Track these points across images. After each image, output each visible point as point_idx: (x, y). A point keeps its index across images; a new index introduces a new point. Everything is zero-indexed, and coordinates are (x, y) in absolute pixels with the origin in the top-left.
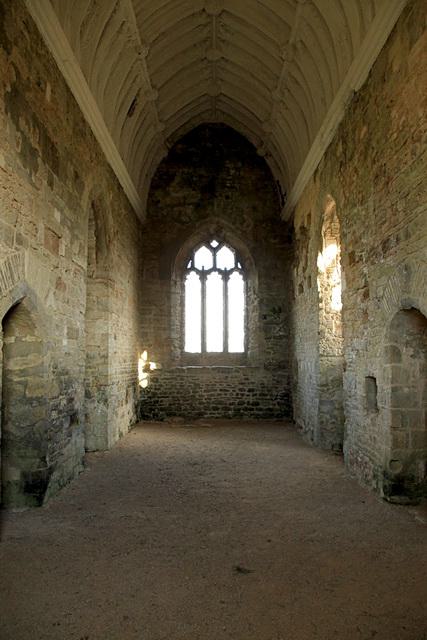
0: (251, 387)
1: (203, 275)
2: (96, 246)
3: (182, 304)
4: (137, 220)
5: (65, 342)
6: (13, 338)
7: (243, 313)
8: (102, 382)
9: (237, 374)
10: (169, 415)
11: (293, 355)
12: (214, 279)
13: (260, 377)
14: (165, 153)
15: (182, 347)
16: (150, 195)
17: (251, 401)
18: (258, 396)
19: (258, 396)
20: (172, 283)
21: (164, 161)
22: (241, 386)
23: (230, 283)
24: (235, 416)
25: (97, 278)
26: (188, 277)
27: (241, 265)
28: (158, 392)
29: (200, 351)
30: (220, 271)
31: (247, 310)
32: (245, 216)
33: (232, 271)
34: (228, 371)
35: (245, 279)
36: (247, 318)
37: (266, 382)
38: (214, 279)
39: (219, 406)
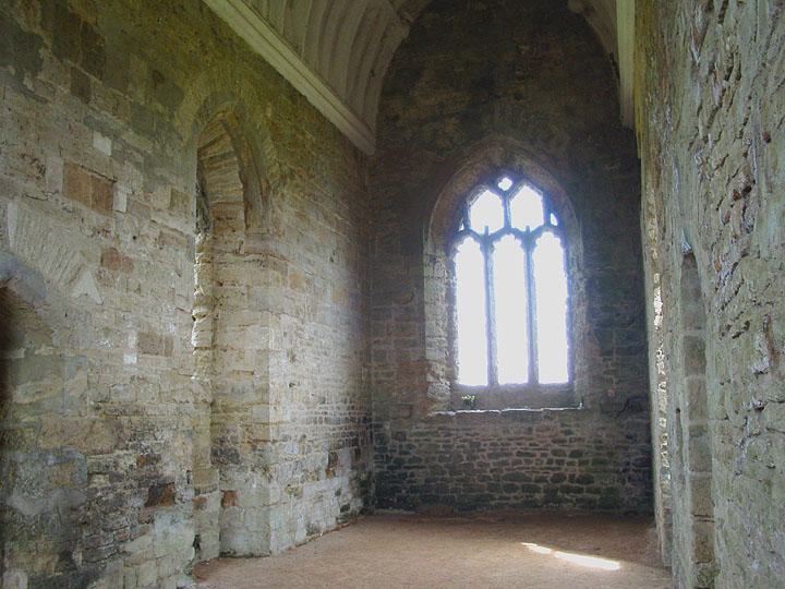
0: (576, 446)
1: (487, 241)
2: (246, 200)
3: (450, 297)
4: (356, 153)
5: (131, 359)
6: (23, 350)
8: (259, 434)
9: (547, 423)
11: (424, 365)
12: (508, 247)
13: (589, 430)
14: (402, 33)
15: (451, 377)
16: (382, 108)
17: (578, 474)
20: (426, 260)
21: (404, 46)
24: (546, 502)
25: (248, 253)
26: (460, 247)
28: (406, 458)
29: (485, 383)
30: (517, 233)
33: (539, 231)
34: (534, 416)
35: (565, 244)
38: (508, 247)
39: (518, 484)
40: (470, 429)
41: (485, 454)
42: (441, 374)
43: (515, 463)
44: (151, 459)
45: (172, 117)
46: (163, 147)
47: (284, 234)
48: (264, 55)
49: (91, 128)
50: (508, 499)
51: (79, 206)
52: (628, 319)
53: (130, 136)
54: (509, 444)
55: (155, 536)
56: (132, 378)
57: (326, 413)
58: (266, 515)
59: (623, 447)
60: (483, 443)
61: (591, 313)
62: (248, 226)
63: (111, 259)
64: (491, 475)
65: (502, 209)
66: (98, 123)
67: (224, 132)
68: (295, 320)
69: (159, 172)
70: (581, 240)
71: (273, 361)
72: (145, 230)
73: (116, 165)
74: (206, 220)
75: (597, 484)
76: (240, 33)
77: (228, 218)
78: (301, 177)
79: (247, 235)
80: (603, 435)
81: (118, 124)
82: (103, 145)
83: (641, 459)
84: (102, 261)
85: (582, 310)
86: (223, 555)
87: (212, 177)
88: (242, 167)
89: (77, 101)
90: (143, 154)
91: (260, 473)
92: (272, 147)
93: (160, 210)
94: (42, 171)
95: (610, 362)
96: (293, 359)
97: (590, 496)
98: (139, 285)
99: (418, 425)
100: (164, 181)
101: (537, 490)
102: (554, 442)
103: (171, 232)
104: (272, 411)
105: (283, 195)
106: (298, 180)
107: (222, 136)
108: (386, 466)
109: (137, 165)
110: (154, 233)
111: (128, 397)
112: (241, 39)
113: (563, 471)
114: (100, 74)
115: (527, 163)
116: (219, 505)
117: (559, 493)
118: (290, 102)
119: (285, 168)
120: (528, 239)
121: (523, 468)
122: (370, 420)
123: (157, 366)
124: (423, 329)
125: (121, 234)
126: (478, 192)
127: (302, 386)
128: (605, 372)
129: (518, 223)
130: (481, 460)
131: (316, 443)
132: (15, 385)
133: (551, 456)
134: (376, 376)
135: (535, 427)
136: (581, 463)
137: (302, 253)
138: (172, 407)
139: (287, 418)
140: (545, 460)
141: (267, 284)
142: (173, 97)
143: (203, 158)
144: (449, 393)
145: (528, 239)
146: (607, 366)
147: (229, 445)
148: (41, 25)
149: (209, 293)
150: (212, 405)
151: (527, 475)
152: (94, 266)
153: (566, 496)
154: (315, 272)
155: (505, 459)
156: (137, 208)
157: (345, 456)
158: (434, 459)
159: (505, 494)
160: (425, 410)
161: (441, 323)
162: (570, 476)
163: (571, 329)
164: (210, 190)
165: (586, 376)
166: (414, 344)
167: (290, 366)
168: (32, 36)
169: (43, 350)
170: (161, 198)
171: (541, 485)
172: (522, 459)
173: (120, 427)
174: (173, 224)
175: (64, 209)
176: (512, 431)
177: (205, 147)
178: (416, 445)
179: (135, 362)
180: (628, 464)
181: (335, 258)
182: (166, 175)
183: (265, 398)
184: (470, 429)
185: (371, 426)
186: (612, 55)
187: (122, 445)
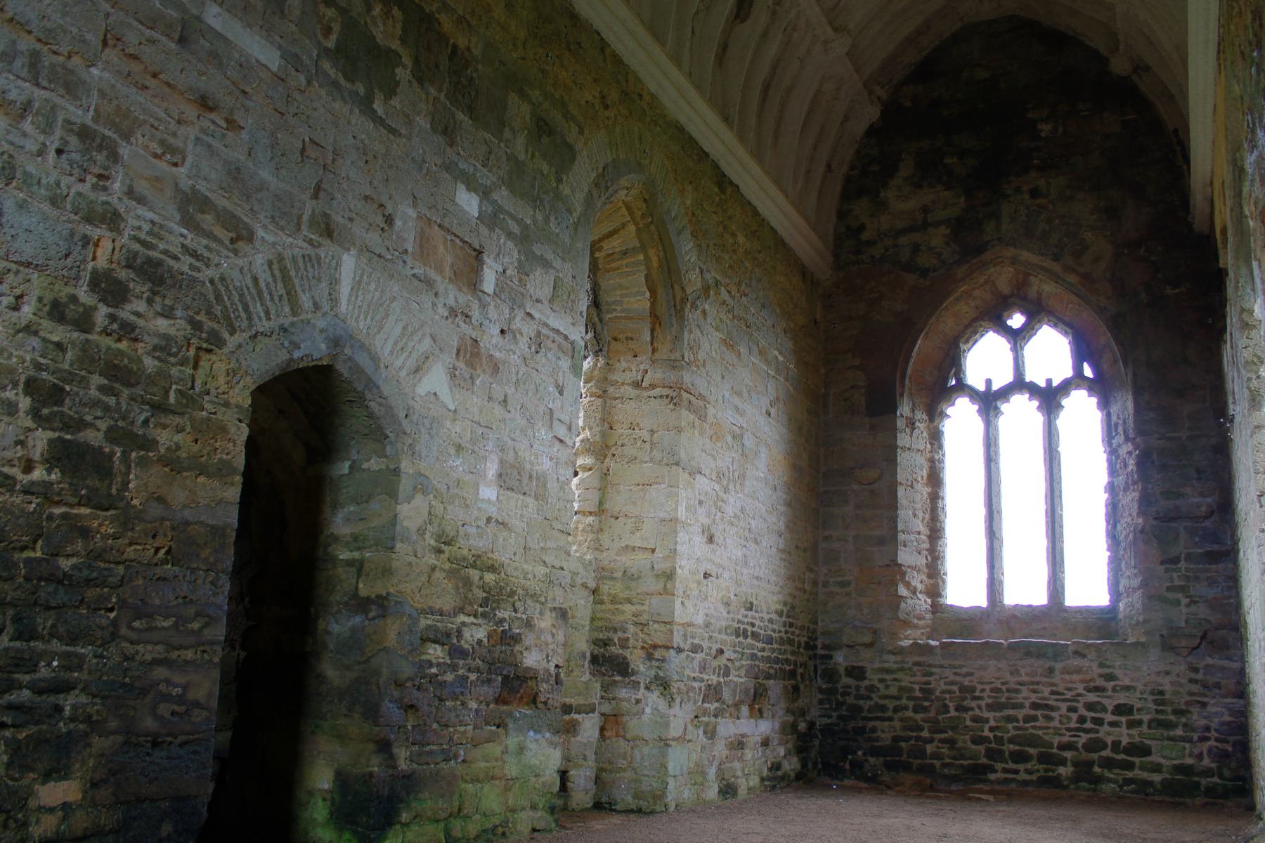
0: (1122, 699)
1: (989, 401)
4: (804, 272)
5: (489, 492)
7: (1102, 497)
9: (1077, 662)
10: (889, 766)
14: (872, 113)
15: (935, 591)
16: (841, 215)
17: (1125, 741)
18: (1145, 728)
19: (1145, 728)
20: (900, 423)
21: (871, 131)
22: (1092, 697)
23: (1063, 421)
25: (653, 386)
27: (1095, 368)
30: (1033, 390)
31: (1111, 488)
32: (1088, 236)
33: (1066, 387)
34: (1057, 652)
35: (1104, 404)
36: (1114, 513)
37: (1167, 688)
39: (1032, 751)
40: (961, 667)
41: (983, 703)
42: (919, 586)
43: (1029, 719)
44: (508, 639)
45: (559, 180)
46: (547, 219)
47: (704, 365)
48: (683, 120)
49: (456, 178)
50: (1016, 772)
51: (433, 275)
52: (1203, 509)
53: (502, 196)
54: (1017, 691)
55: (506, 747)
56: (489, 520)
57: (753, 625)
58: (664, 755)
59: (1199, 702)
60: (979, 687)
61: (1145, 501)
62: (654, 351)
63: (471, 352)
64: (991, 735)
65: (1009, 356)
66: (463, 173)
67: (629, 219)
68: (717, 487)
69: (538, 249)
70: (1130, 398)
71: (682, 536)
72: (517, 323)
73: (484, 230)
74: (596, 337)
75: (1155, 758)
76: (653, 87)
77: (627, 339)
78: (729, 292)
79: (653, 362)
80: (1166, 684)
81: (486, 178)
82: (469, 203)
83: (1229, 723)
84: (458, 354)
85: (1130, 499)
86: (598, 806)
87: (607, 282)
88: (648, 268)
89: (440, 139)
90: (519, 222)
91: (657, 693)
92: (691, 245)
93: (537, 301)
94: (389, 220)
95: (1175, 575)
96: (711, 540)
97: (1145, 775)
98: (505, 396)
99: (885, 657)
100: (546, 264)
101: (1063, 762)
102: (1089, 691)
103: (551, 334)
104: (678, 605)
105: (704, 312)
106: (725, 295)
107: (624, 225)
108: (835, 714)
109: (510, 235)
110: (528, 329)
111: (480, 544)
112: (653, 96)
113: (1100, 735)
114: (471, 110)
115: (1049, 288)
116: (596, 734)
117: (1097, 769)
118: (716, 190)
119: (708, 276)
120: (1050, 398)
121: (1040, 728)
122: (815, 647)
123: (521, 510)
124: (894, 519)
125: (486, 323)
126: (975, 333)
127: (721, 580)
128: (1168, 589)
129: (1036, 374)
130: (977, 712)
131: (737, 664)
132: (335, 506)
133: (1083, 712)
134: (825, 584)
135: (1058, 666)
136: (1132, 724)
137: (727, 395)
138: (541, 570)
139: (700, 620)
140: (1074, 716)
141: (679, 430)
142: (564, 157)
143: (597, 255)
144: (929, 616)
145: (1050, 398)
146: (1172, 580)
147: (615, 650)
148: (400, 39)
149: (597, 438)
150: (594, 592)
151: (1046, 737)
152: (449, 358)
153: (1107, 774)
154: (745, 425)
155: (1011, 712)
156: (511, 294)
157: (775, 688)
158: (906, 708)
159: (1011, 765)
160: (894, 635)
161: (920, 514)
162: (1113, 742)
163: (1115, 526)
164: (605, 298)
165: (1139, 593)
166: (881, 542)
167: (707, 548)
168: (389, 50)
169: (374, 464)
170: (539, 284)
171: (1068, 755)
172: (1039, 713)
173: (467, 582)
174: (555, 322)
175: (414, 275)
176: (1022, 671)
177: (600, 240)
178: (881, 686)
179: (494, 498)
180: (1208, 729)
181: (773, 411)
182: (550, 256)
183: (669, 586)
184: (961, 667)
185: (815, 655)
186: (1176, 131)
187: (468, 608)
